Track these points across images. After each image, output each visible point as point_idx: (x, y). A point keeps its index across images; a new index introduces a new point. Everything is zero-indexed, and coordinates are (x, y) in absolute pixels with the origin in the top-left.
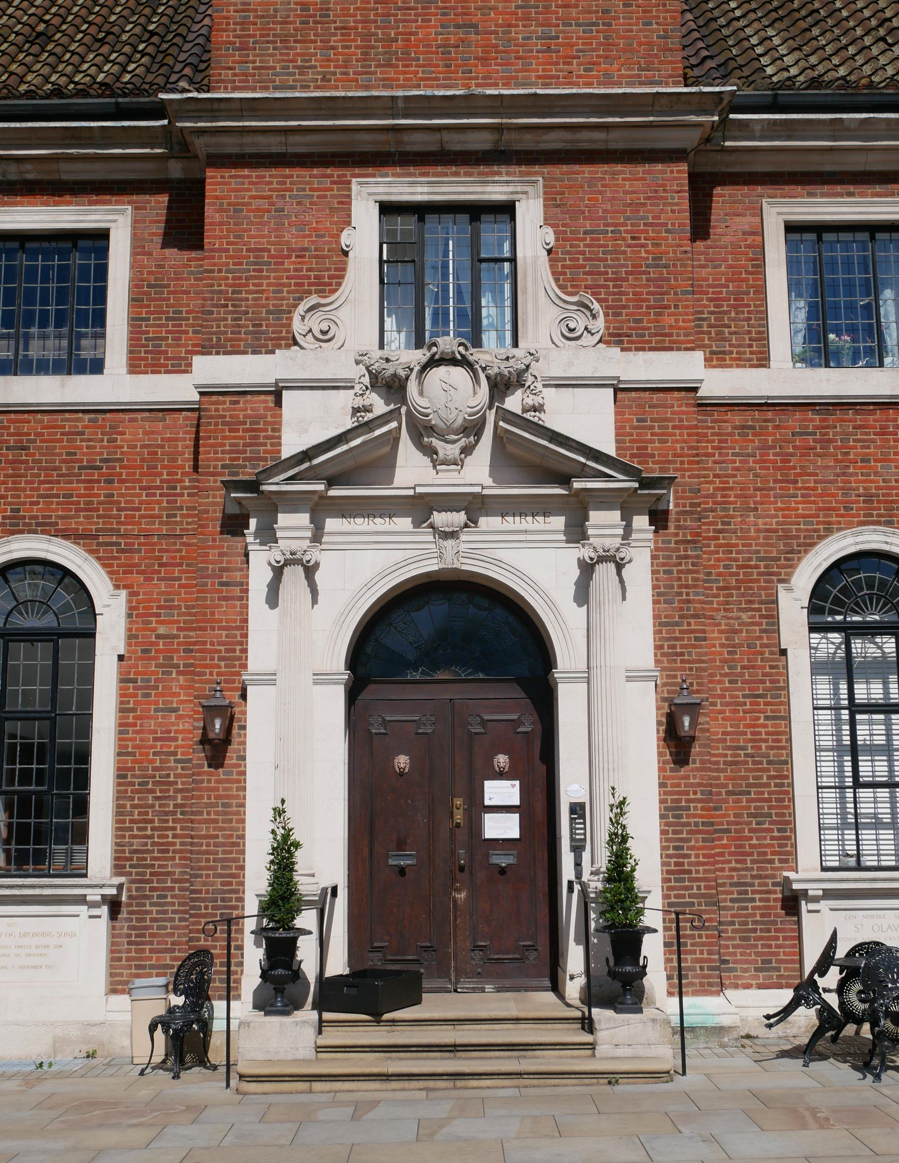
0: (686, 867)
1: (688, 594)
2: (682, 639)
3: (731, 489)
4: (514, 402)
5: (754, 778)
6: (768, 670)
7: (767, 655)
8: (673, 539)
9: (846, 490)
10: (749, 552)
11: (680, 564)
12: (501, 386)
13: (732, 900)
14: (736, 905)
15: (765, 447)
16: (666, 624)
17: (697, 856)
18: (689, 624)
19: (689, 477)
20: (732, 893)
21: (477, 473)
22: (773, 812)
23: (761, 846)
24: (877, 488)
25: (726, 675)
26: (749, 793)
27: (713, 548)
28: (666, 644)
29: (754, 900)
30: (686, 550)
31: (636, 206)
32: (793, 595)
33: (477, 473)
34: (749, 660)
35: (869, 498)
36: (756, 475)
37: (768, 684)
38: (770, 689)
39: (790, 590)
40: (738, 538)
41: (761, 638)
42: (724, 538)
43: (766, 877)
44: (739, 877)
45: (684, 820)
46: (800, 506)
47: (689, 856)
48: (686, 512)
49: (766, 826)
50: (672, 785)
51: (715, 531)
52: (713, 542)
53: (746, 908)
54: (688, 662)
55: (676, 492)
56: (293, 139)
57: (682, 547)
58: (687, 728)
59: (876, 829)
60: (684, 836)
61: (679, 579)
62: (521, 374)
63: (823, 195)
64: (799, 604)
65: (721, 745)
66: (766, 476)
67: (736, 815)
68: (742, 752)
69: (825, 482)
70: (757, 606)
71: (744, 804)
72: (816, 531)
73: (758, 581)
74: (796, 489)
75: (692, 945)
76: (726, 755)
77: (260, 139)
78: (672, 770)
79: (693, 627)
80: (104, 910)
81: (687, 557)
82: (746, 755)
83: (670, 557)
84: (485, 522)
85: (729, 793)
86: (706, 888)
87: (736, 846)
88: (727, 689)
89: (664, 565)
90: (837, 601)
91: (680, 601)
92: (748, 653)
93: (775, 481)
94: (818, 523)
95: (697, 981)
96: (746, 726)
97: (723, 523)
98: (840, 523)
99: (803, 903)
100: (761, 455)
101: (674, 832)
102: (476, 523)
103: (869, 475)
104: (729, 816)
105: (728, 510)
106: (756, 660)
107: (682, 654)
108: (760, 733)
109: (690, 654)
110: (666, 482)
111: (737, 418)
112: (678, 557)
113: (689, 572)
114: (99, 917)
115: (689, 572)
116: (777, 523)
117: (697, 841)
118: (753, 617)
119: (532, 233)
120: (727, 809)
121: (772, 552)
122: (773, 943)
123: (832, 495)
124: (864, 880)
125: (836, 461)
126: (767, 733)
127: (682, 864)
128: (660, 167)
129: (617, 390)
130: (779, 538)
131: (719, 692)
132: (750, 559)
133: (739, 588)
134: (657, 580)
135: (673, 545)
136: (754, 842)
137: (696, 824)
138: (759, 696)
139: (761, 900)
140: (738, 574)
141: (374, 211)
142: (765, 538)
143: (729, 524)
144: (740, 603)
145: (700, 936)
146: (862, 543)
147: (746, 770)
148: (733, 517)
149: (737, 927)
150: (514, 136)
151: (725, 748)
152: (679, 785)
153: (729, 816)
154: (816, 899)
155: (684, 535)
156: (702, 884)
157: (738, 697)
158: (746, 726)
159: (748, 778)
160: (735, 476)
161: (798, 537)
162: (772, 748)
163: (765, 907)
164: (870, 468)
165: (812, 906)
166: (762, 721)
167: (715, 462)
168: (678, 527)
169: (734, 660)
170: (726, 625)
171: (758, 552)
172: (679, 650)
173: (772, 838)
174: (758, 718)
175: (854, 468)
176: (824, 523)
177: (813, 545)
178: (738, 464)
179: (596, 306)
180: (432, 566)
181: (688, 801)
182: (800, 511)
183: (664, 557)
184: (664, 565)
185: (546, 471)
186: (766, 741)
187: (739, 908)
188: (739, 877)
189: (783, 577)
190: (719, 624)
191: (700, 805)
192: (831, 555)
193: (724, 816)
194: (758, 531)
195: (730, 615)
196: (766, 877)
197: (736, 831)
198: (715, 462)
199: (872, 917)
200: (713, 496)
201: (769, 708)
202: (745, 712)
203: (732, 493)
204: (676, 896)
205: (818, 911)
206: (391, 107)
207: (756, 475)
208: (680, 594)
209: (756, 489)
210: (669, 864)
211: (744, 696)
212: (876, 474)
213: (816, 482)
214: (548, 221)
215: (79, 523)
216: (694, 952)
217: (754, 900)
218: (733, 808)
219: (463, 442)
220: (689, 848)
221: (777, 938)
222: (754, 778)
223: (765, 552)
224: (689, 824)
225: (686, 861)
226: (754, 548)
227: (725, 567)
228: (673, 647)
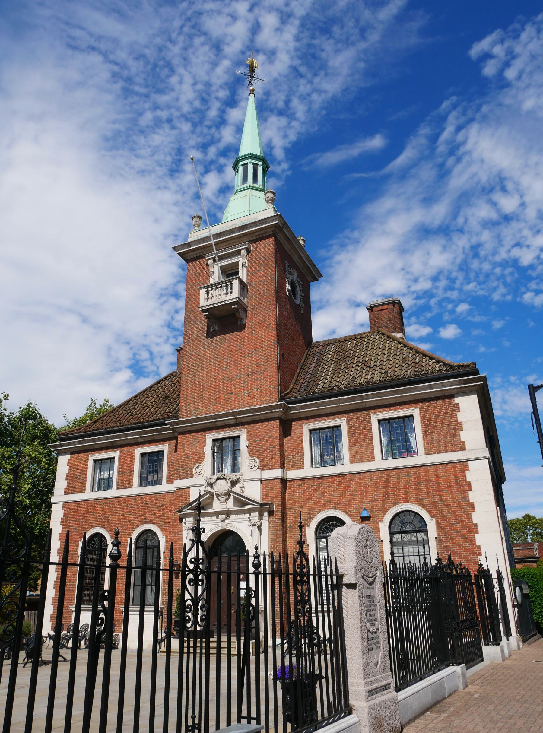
4: (237, 489)
9: (324, 500)
12: (234, 483)
15: (304, 490)
21: (230, 505)
31: (267, 433)
33: (230, 505)
35: (330, 502)
56: (194, 427)
62: (238, 479)
63: (318, 421)
77: (188, 428)
84: (232, 517)
90: (324, 530)
102: (229, 517)
111: (297, 483)
119: (244, 443)
128: (272, 422)
129: (261, 481)
141: (211, 441)
150: (239, 420)
179: (257, 459)
180: (220, 528)
185: (242, 502)
206: (211, 418)
214: (247, 439)
215: (157, 520)
219: (226, 497)
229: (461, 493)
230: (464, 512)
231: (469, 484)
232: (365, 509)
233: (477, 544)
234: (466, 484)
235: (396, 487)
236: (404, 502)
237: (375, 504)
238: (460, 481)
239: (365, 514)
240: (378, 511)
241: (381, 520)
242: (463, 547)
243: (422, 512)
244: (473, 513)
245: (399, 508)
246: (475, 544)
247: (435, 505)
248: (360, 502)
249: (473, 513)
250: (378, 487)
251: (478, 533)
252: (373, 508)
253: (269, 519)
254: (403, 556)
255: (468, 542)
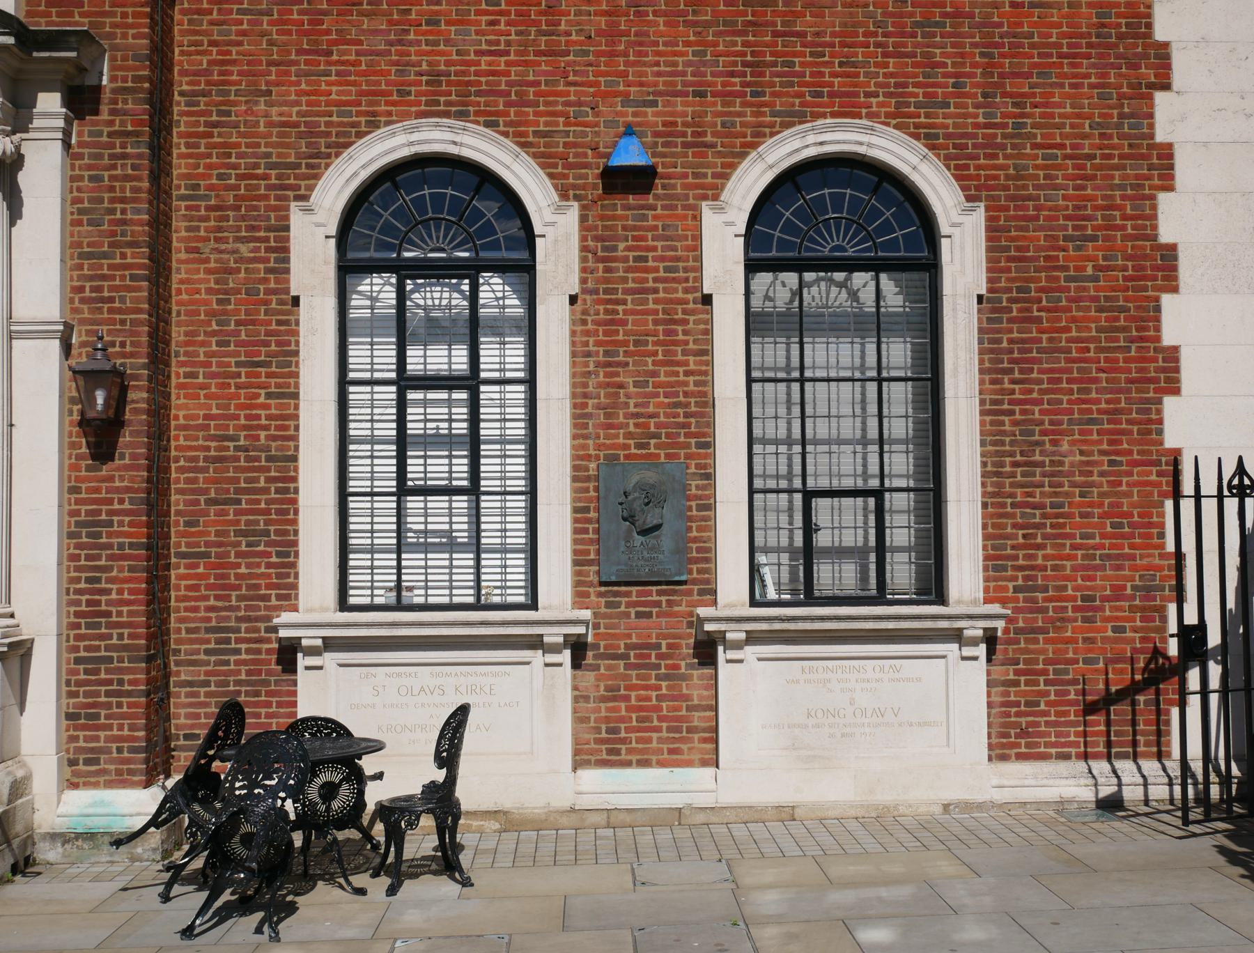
0: (104, 608)
1: (123, 212)
2: (113, 278)
3: (234, 62)
5: (247, 481)
6: (274, 327)
7: (274, 305)
8: (106, 130)
10: (255, 155)
11: (114, 167)
13: (207, 652)
14: (213, 658)
16: (89, 256)
17: (120, 592)
18: (123, 256)
19: (134, 37)
20: (208, 641)
22: (272, 528)
23: (251, 576)
24: (448, 63)
25: (214, 333)
26: (239, 502)
27: (202, 149)
28: (88, 285)
29: (238, 651)
30: (123, 146)
32: (314, 218)
34: (247, 313)
35: (435, 77)
36: (271, 43)
37: (273, 347)
38: (275, 354)
39: (309, 210)
40: (240, 135)
41: (266, 280)
42: (220, 135)
43: (257, 619)
44: (219, 619)
45: (104, 540)
46: (334, 89)
47: (108, 592)
48: (125, 89)
49: (261, 548)
50: (89, 490)
51: (207, 124)
52: (203, 141)
53: (227, 663)
54: (120, 311)
55: (113, 59)
57: (118, 142)
58: (99, 408)
59: (451, 553)
60: (103, 563)
61: (112, 189)
64: (321, 232)
65: (201, 434)
66: (285, 44)
67: (218, 533)
68: (231, 444)
69: (371, 53)
70: (262, 234)
71: (231, 517)
72: (353, 125)
73: (266, 197)
74: (329, 63)
75: (107, 717)
76: (208, 449)
78: (88, 468)
79: (129, 260)
80: (981, 650)
81: (124, 156)
82: (237, 448)
83: (100, 156)
85: (210, 502)
86: (131, 636)
87: (217, 577)
88: (213, 354)
89: (89, 167)
91: (111, 222)
92: (246, 302)
93: (299, 52)
94: (359, 114)
95: (112, 767)
96: (238, 407)
97: (220, 113)
98: (390, 114)
99: (720, 649)
100: (280, 13)
101: (88, 558)
103: (437, 43)
104: (209, 534)
105: (228, 93)
106: (258, 313)
107: (111, 300)
108: (258, 417)
109: (122, 299)
110: (73, 39)
112: (112, 157)
113: (126, 178)
114: (560, 665)
115: (126, 178)
116: (298, 113)
117: (121, 570)
118: (257, 250)
120: (206, 524)
121: (289, 155)
122: (263, 711)
123: (382, 73)
124: (822, 619)
125: (390, 22)
126: (269, 417)
127: (98, 603)
130: (300, 135)
131: (202, 358)
132: (256, 166)
133: (238, 208)
134: (79, 190)
135: (105, 139)
136: (243, 570)
137: (121, 546)
138: (259, 364)
139: (248, 651)
140: (237, 187)
142: (280, 135)
143: (228, 114)
144: (239, 229)
145: (119, 705)
146: (420, 142)
147: (236, 469)
148: (235, 104)
149: (213, 688)
151: (206, 439)
152: (98, 490)
153: (209, 534)
154: (738, 646)
155: (123, 123)
156: (126, 631)
157: (229, 365)
158: (238, 407)
159: (237, 480)
160: (240, 44)
161: (328, 134)
162: (275, 438)
163: (254, 662)
164: (439, 33)
165: (732, 655)
166: (262, 400)
167: (211, 23)
168: (113, 112)
169: (225, 312)
170: (216, 261)
171: (268, 155)
172: (106, 294)
173: (269, 566)
174: (258, 396)
175: (416, 33)
176: (367, 113)
177: (347, 145)
178: (245, 26)
181: (111, 513)
182: (334, 96)
183: (91, 156)
184: (89, 167)
186: (266, 428)
187: (217, 663)
188: (219, 619)
189: (302, 192)
190: (207, 261)
191: (127, 519)
192: (371, 161)
193: (201, 534)
194: (270, 124)
195: (223, 247)
196: (257, 619)
197: (218, 555)
198: (211, 23)
199: (399, 675)
200: (207, 72)
201: (273, 381)
202: (238, 387)
203: (235, 69)
204: (87, 649)
205: (320, 668)
207: (271, 43)
208: (112, 211)
209: (270, 63)
210: (78, 603)
211: (238, 364)
212: (448, 42)
213: (358, 53)
216: (110, 727)
217: (238, 651)
218: (215, 523)
220: (109, 581)
221: (269, 704)
222: (247, 481)
223: (279, 155)
224: (110, 546)
225: (104, 598)
226: (263, 149)
227: (220, 177)
228: (99, 289)
229: (1121, 96)
230: (1122, 187)
231: (1162, 54)
232: (629, 131)
233: (1168, 340)
234: (1146, 56)
235: (802, 35)
236: (834, 115)
237: (684, 108)
238: (1120, 36)
239: (631, 155)
240: (699, 146)
241: (713, 193)
242: (1100, 350)
243: (924, 167)
244: (1163, 197)
245: (811, 139)
246: (1158, 339)
247: (990, 143)
248: (605, 95)
249: (1163, 197)
250: (707, 24)
251: (1175, 290)
252: (669, 131)
253: (67, 133)
254: (880, 381)
255: (1125, 329)
